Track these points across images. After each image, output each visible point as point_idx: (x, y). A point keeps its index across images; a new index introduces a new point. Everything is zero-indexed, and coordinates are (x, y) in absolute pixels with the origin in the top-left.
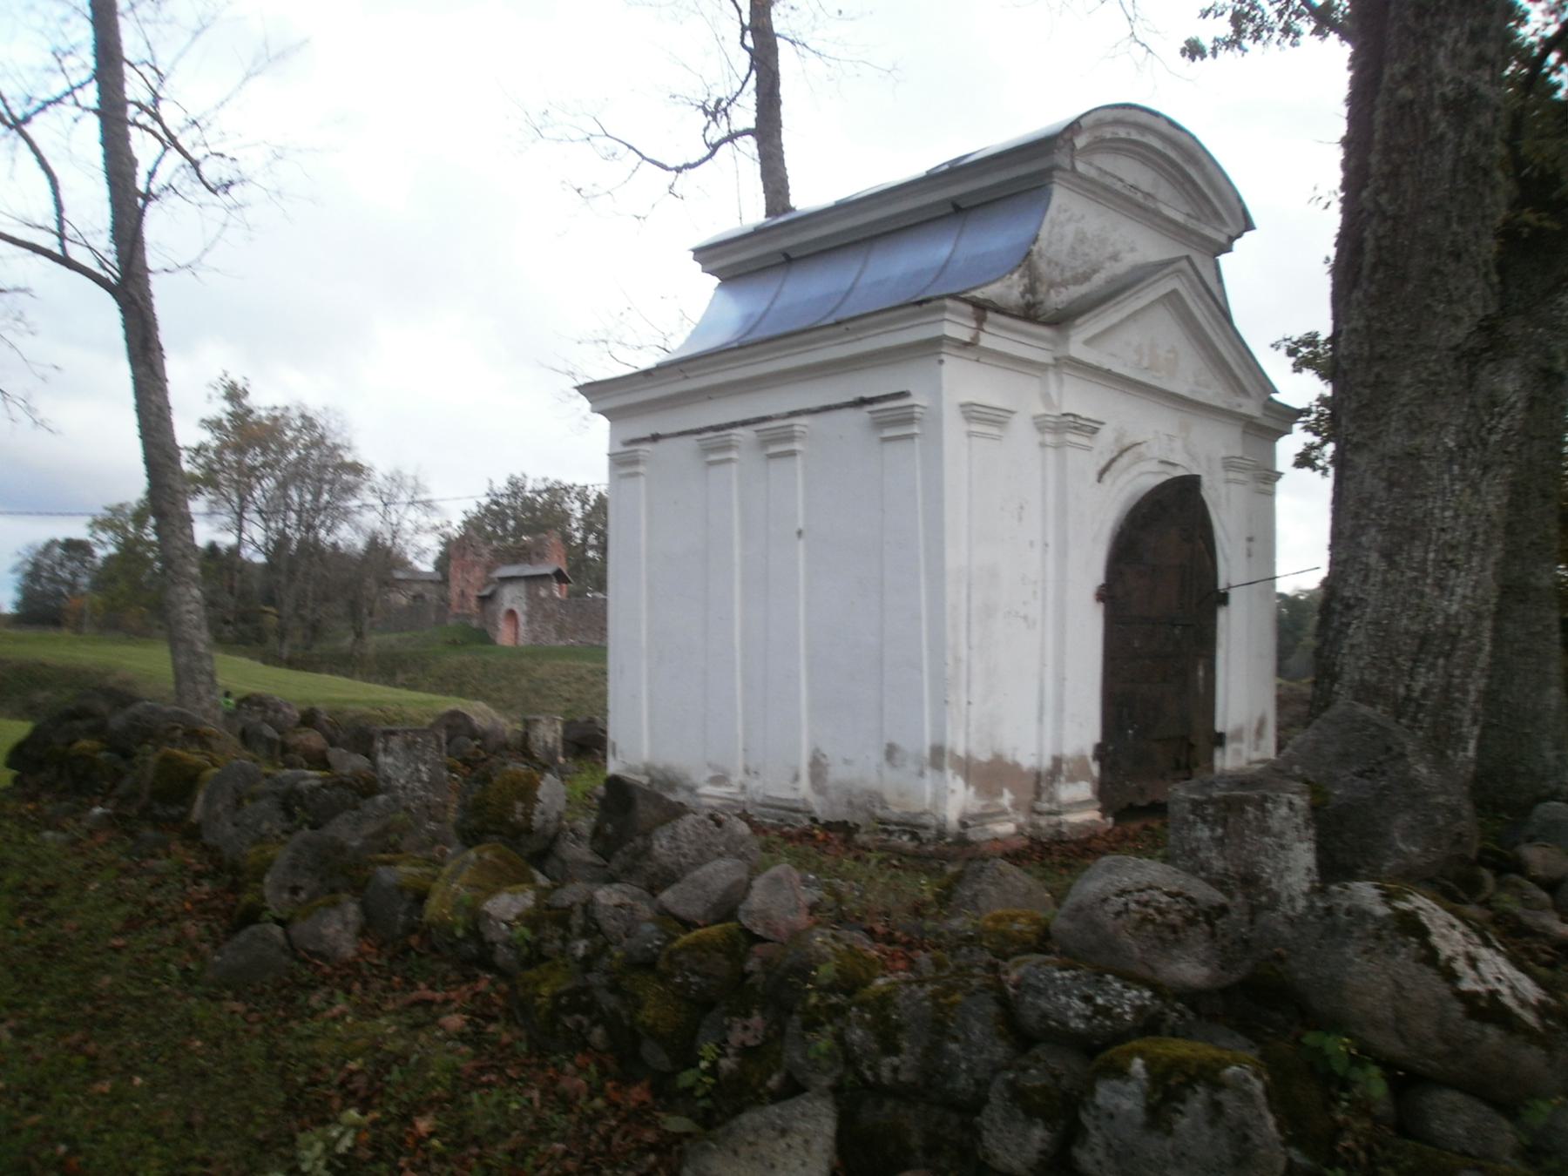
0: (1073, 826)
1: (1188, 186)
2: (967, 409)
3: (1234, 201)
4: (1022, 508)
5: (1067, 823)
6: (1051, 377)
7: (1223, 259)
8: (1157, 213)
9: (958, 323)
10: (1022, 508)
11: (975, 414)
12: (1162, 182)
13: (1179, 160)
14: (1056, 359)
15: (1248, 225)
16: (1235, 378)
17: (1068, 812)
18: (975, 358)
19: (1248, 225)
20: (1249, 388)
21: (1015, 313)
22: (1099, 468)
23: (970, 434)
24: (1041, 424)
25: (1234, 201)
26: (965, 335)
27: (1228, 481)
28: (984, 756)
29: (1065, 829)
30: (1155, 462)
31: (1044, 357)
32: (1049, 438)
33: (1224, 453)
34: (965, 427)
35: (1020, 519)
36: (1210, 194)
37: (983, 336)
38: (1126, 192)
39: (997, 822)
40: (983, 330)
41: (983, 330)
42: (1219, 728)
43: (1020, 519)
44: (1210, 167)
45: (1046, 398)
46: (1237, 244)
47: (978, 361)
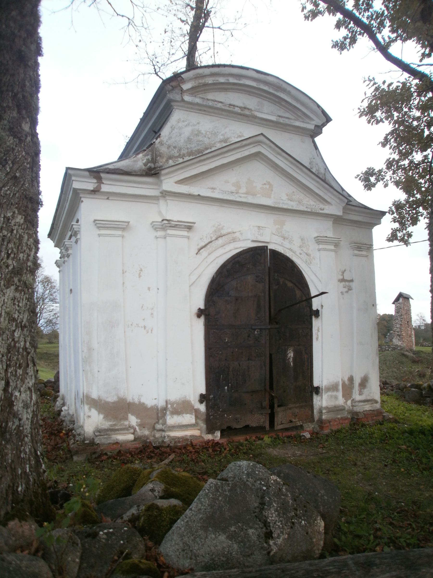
0: (174, 438)
1: (283, 103)
2: (316, 239)
3: (316, 108)
4: (141, 270)
5: (168, 436)
6: (162, 202)
7: (317, 139)
8: (255, 117)
9: (83, 181)
10: (141, 270)
11: (320, 240)
12: (265, 103)
13: (271, 91)
14: (161, 193)
15: (328, 119)
16: (317, 194)
17: (170, 431)
18: (106, 198)
19: (328, 119)
20: (329, 200)
21: (139, 173)
22: (199, 247)
23: (99, 235)
24: (155, 227)
25: (316, 108)
26: (91, 187)
27: (319, 250)
28: (111, 398)
29: (166, 440)
30: (249, 241)
31: (155, 193)
32: (161, 233)
33: (316, 235)
34: (316, 246)
35: (140, 276)
36: (294, 103)
37: (102, 186)
38: (227, 108)
39: (120, 434)
40: (103, 183)
41: (103, 183)
42: (315, 384)
43: (140, 276)
44: (293, 92)
45: (160, 213)
46: (324, 129)
47: (108, 199)
